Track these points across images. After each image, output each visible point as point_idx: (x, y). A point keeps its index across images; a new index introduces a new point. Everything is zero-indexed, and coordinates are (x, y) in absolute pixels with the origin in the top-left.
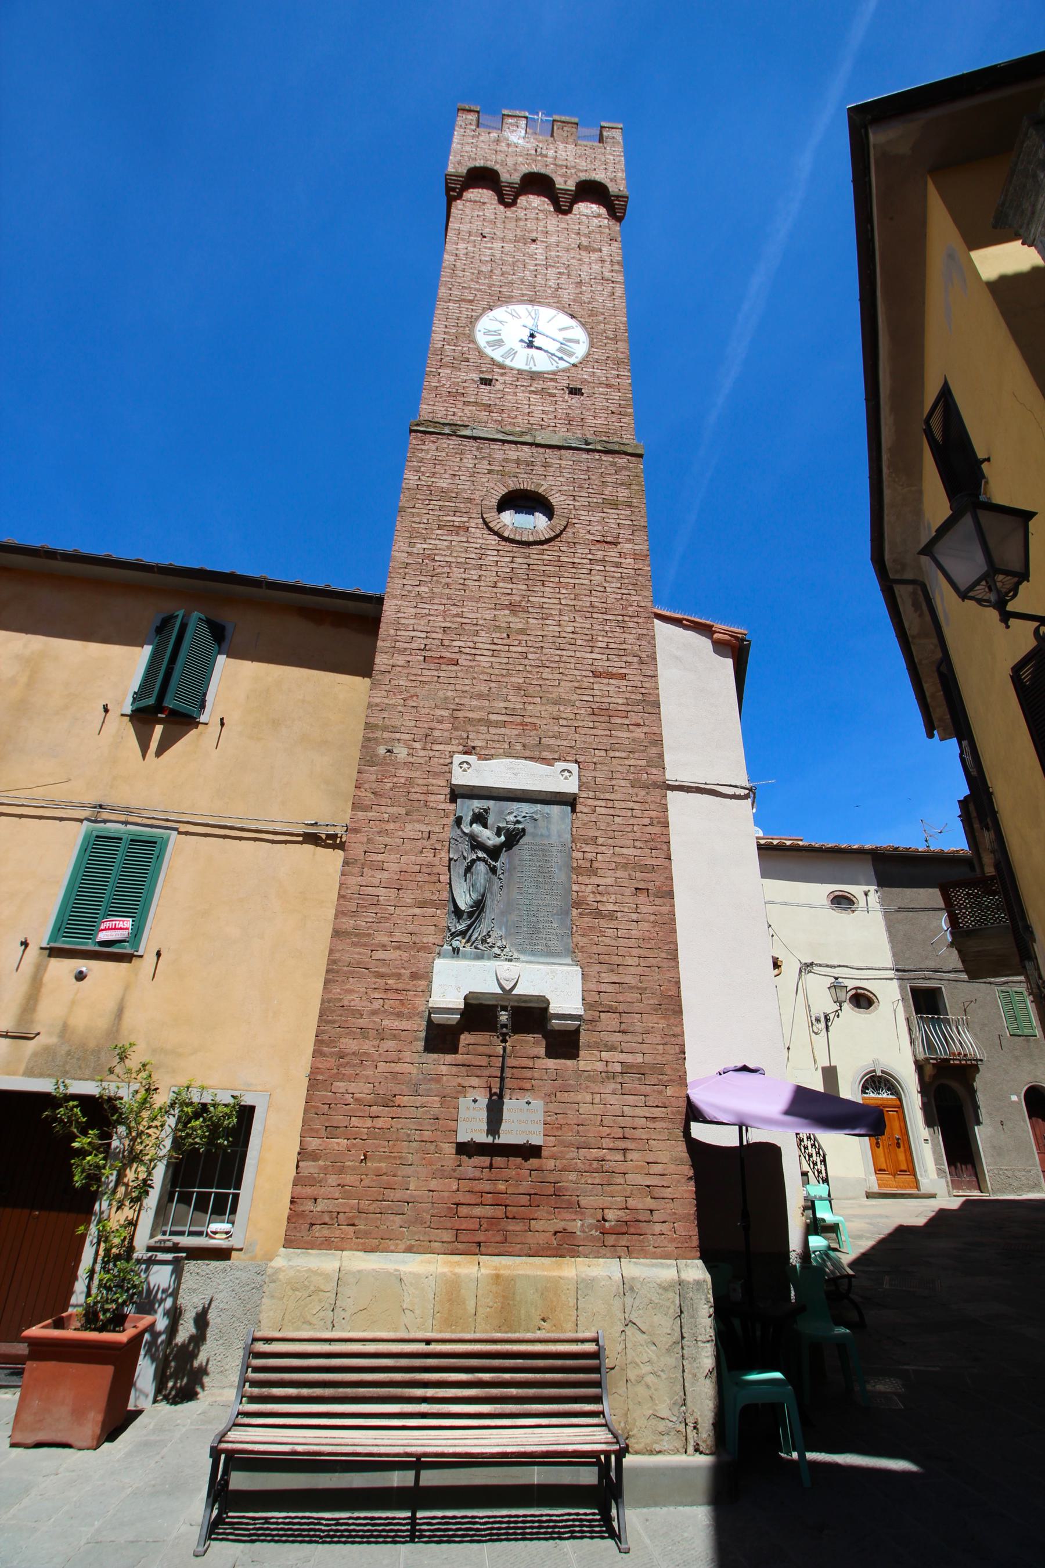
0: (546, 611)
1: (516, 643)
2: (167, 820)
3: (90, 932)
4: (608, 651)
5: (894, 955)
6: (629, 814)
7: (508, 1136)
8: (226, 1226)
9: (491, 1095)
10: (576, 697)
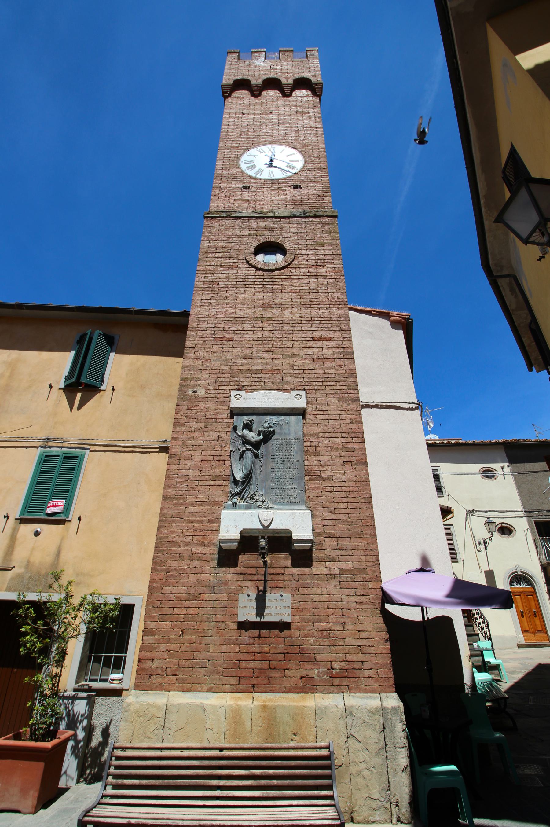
0: (284, 306)
1: (267, 325)
2: (84, 444)
3: (42, 509)
4: (321, 326)
5: (523, 503)
6: (338, 418)
7: (268, 617)
8: (119, 676)
9: (259, 592)
10: (303, 353)
